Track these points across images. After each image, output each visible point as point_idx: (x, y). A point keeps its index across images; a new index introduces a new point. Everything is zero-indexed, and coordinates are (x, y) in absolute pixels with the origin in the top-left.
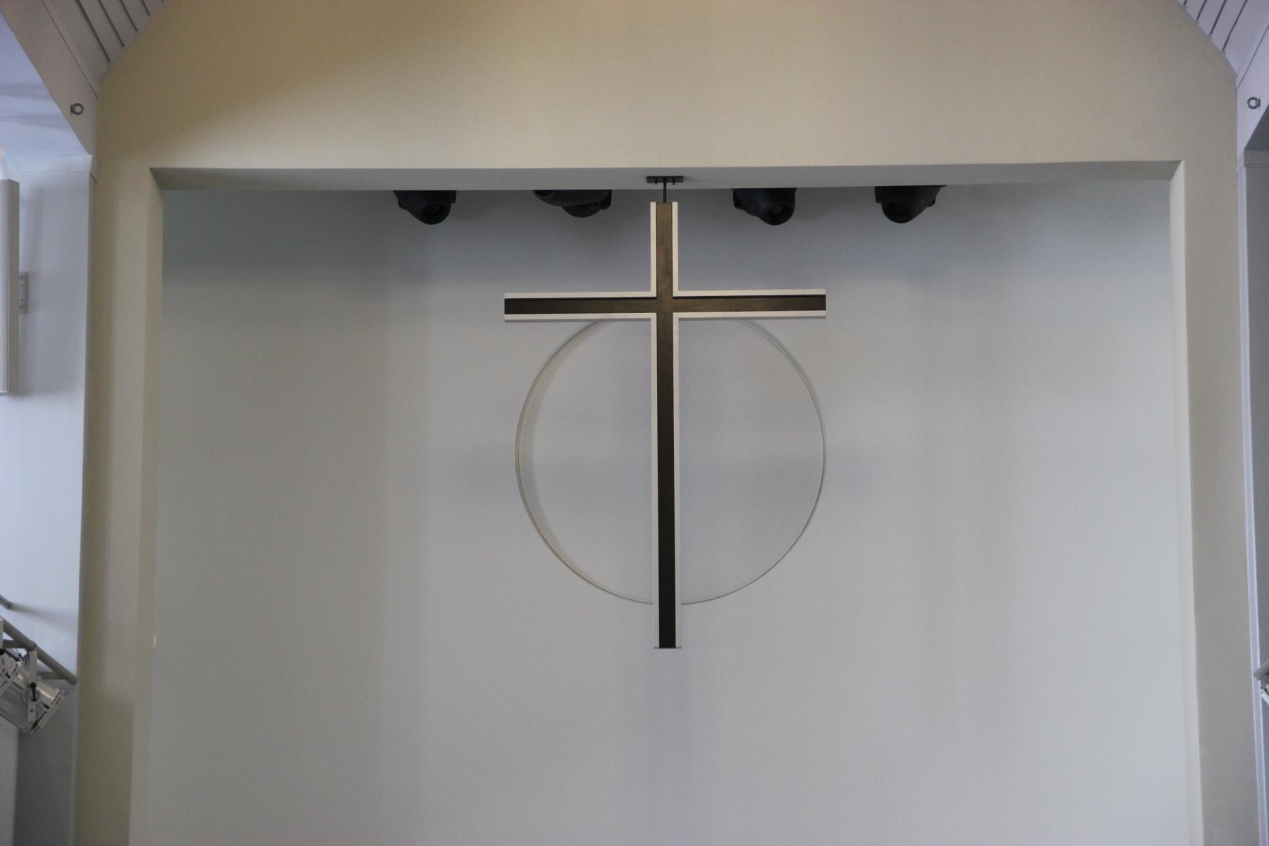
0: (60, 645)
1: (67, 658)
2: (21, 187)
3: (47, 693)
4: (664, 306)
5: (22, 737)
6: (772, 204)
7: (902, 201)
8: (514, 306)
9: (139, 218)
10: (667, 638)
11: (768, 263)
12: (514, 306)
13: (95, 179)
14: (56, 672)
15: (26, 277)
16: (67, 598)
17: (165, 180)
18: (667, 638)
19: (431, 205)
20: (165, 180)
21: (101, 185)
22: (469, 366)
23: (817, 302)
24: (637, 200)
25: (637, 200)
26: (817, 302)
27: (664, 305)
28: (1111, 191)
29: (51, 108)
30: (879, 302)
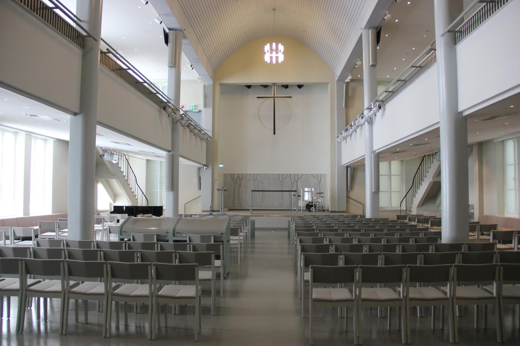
0: (210, 134)
1: (211, 136)
2: (164, 208)
3: (209, 139)
4: (274, 97)
5: (207, 144)
6: (286, 86)
7: (300, 86)
8: (258, 98)
9: (218, 88)
10: (274, 133)
11: (285, 92)
12: (258, 98)
13: (213, 84)
14: (210, 137)
15: (175, 67)
16: (211, 129)
17: (221, 84)
18: (274, 133)
19: (249, 87)
20: (221, 84)
21: (214, 85)
22: (252, 103)
23: (291, 97)
24: (271, 86)
25: (271, 86)
26: (291, 97)
27: (274, 97)
28: (322, 85)
29: (209, 77)
30: (297, 96)
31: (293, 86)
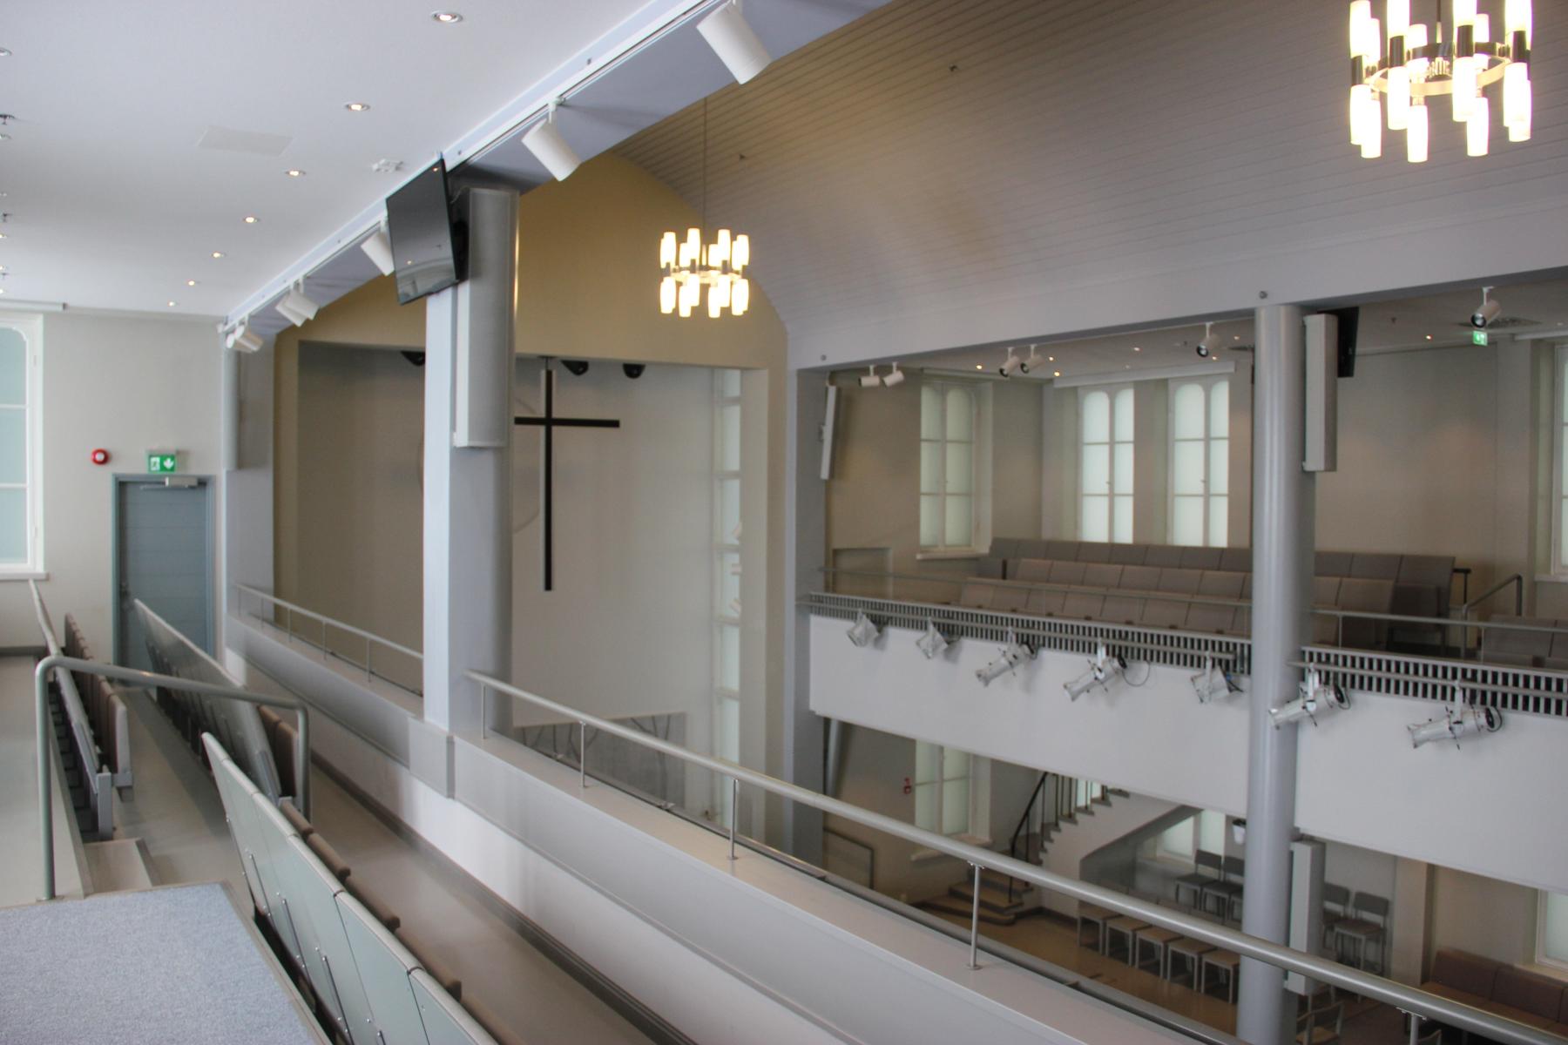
31: (604, 364)
